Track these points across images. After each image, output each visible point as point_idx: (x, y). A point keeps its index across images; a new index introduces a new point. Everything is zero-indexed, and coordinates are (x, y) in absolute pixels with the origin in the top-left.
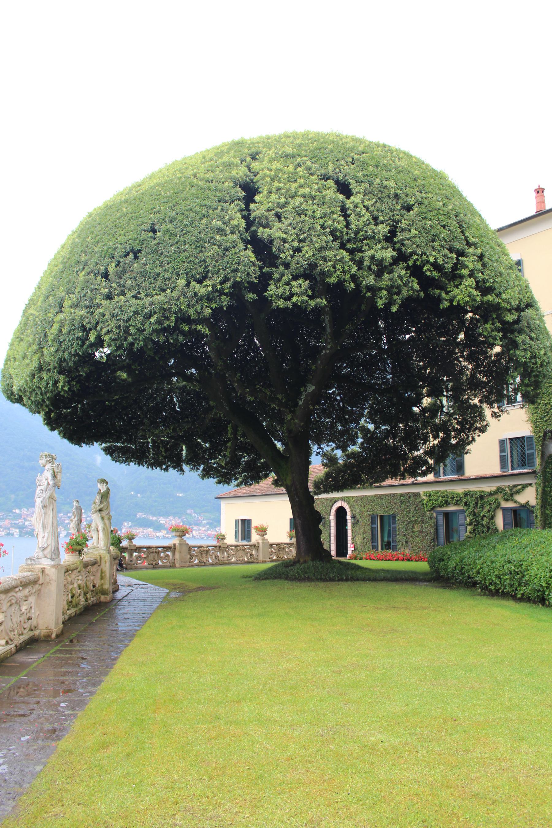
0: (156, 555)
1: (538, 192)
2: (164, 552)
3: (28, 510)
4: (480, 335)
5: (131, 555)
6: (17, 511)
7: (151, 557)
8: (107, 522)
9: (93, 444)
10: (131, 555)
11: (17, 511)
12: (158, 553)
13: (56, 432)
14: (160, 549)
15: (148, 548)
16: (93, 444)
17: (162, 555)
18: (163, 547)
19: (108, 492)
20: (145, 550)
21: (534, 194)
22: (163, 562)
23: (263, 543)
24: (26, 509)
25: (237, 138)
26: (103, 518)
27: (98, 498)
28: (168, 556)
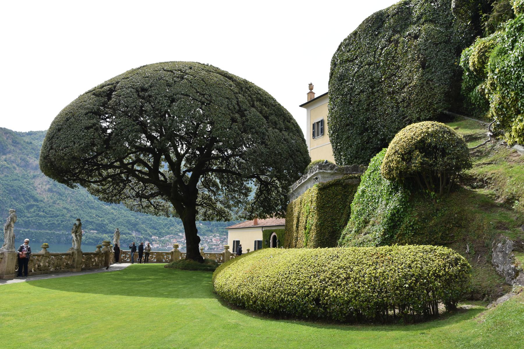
15: (157, 253)
26: (76, 236)
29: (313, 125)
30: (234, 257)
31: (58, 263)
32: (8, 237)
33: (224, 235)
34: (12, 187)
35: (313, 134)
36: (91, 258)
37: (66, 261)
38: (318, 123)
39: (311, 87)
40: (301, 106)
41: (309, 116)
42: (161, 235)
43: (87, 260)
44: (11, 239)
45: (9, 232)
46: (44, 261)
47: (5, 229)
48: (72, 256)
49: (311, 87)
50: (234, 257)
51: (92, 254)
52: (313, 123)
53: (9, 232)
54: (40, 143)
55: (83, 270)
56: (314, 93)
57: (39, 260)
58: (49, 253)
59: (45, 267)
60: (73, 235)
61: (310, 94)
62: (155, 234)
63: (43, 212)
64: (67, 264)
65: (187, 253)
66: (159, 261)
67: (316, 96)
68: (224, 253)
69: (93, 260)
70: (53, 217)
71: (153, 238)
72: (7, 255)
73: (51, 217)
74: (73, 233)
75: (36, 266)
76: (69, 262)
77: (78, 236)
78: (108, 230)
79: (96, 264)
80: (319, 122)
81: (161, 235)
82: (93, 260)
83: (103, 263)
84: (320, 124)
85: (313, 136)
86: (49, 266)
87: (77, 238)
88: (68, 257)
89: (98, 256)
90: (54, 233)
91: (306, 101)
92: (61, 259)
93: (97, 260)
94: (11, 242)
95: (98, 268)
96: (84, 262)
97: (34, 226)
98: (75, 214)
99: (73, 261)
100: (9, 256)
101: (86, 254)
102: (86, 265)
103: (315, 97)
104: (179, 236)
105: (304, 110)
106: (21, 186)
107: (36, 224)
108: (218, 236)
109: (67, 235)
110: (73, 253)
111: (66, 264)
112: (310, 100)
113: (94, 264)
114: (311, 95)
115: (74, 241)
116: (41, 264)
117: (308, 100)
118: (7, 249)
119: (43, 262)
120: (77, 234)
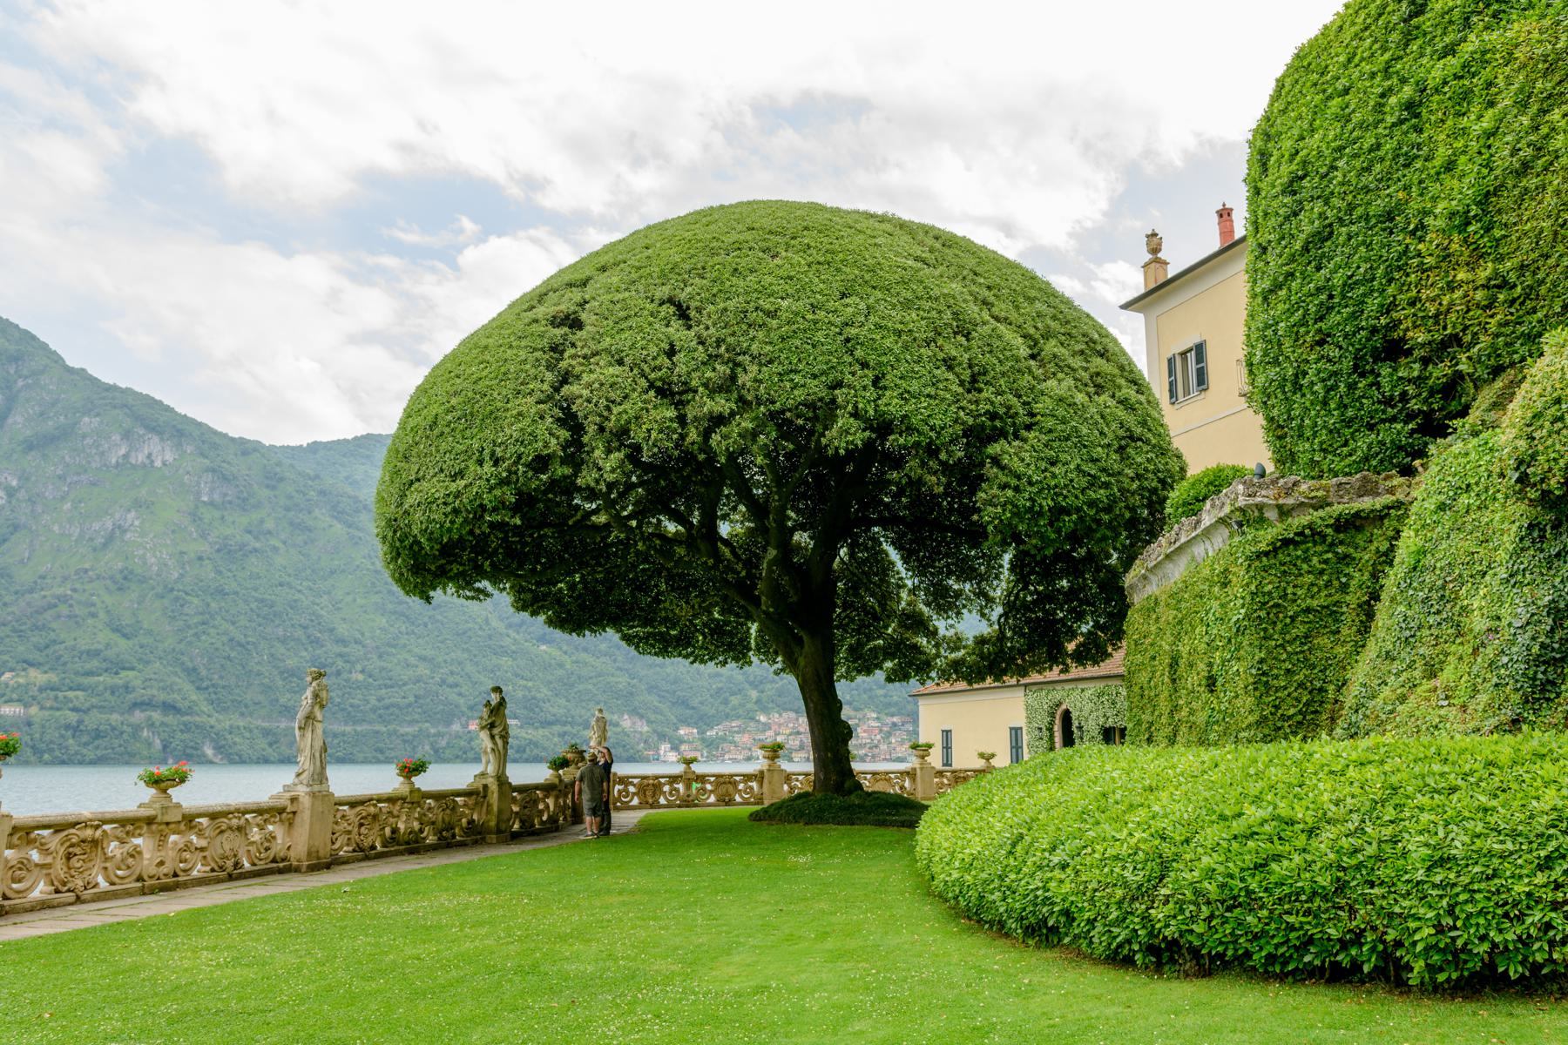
0: (731, 788)
1: (1221, 216)
2: (745, 782)
3: (780, 715)
4: (675, 502)
5: (688, 787)
6: (763, 719)
7: (722, 790)
8: (500, 742)
9: (604, 631)
10: (688, 787)
11: (763, 719)
12: (735, 784)
13: (542, 618)
14: (737, 778)
15: (718, 776)
16: (604, 631)
17: (741, 786)
18: (975, 771)
19: (502, 703)
20: (712, 779)
21: (1216, 218)
22: (742, 797)
23: (922, 769)
24: (777, 715)
25: (1278, 62)
26: (492, 737)
27: (485, 712)
28: (751, 788)
29: (1170, 361)
30: (709, 787)
31: (447, 819)
32: (307, 752)
33: (892, 715)
34: (272, 607)
35: (1171, 391)
36: (536, 802)
37: (468, 813)
38: (1184, 354)
39: (1154, 243)
40: (1126, 306)
41: (1154, 338)
42: (703, 722)
43: (525, 807)
44: (317, 755)
45: (309, 735)
46: (408, 816)
47: (300, 728)
48: (485, 797)
49: (1154, 243)
50: (946, 781)
51: (537, 787)
52: (1170, 355)
53: (309, 735)
54: (370, 480)
55: (515, 837)
56: (1166, 263)
57: (395, 813)
58: (419, 790)
59: (411, 833)
60: (484, 735)
61: (1153, 265)
62: (685, 722)
63: (362, 672)
64: (471, 822)
65: (816, 774)
66: (726, 801)
67: (1172, 272)
68: (915, 769)
69: (541, 806)
70: (392, 687)
71: (682, 732)
72: (306, 801)
73: (386, 687)
74: (483, 728)
75: (388, 831)
76: (475, 817)
77: (497, 738)
78: (551, 718)
79: (549, 817)
80: (1190, 350)
81: (703, 722)
82: (541, 806)
83: (569, 812)
84: (1192, 357)
85: (1171, 397)
86: (421, 831)
87: (495, 743)
88: (471, 801)
89: (555, 793)
90: (395, 732)
91: (1142, 291)
92: (453, 809)
93: (552, 808)
94: (318, 763)
95: (557, 829)
96: (517, 813)
97: (339, 715)
98: (452, 673)
99: (488, 812)
100: (313, 805)
101: (523, 789)
102: (522, 822)
103: (1170, 276)
104: (759, 721)
105: (1137, 320)
106: (295, 601)
107: (343, 710)
108: (874, 719)
109: (434, 735)
110: (485, 787)
111: (469, 823)
112: (1152, 285)
113: (545, 818)
114: (1156, 269)
115: (485, 752)
116: (401, 826)
117: (1146, 285)
118: (308, 785)
119: (404, 818)
120: (496, 731)
